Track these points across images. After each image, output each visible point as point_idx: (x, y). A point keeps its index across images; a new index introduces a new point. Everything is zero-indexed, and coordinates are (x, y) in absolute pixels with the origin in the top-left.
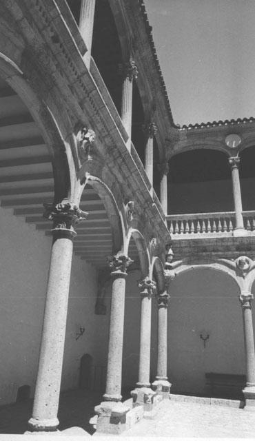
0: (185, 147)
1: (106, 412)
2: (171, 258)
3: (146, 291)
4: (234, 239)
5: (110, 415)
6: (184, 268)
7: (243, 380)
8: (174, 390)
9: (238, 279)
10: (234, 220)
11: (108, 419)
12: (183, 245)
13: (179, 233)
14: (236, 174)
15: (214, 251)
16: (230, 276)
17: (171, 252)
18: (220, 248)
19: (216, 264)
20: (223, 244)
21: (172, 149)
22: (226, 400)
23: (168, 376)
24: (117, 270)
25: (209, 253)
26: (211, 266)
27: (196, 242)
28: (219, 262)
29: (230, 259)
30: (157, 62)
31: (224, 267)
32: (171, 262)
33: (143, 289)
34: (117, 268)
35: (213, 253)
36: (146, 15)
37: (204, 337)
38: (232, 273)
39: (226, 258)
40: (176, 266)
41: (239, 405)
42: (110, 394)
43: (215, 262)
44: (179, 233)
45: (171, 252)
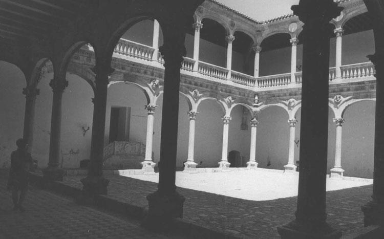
9: (289, 111)
23: (229, 161)
26: (277, 104)
28: (281, 103)
43: (278, 102)
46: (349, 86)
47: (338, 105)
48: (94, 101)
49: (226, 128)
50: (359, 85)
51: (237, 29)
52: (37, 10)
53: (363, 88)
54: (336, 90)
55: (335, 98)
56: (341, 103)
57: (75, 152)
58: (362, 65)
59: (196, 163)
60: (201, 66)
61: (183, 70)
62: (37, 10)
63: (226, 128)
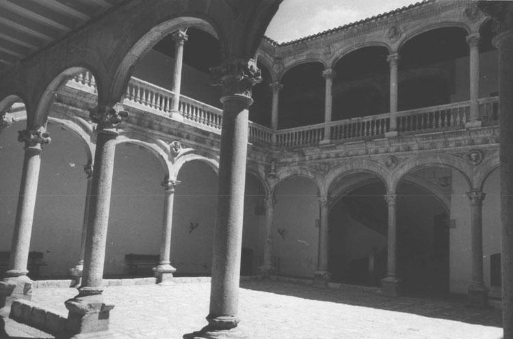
1: (94, 308)
3: (38, 147)
4: (169, 121)
5: (98, 311)
7: (157, 260)
8: (176, 275)
9: (169, 163)
10: (172, 101)
11: (97, 316)
14: (181, 50)
15: (71, 105)
18: (79, 104)
19: (70, 121)
20: (84, 99)
22: (56, 281)
23: (170, 260)
24: (113, 127)
25: (65, 106)
26: (64, 121)
28: (74, 120)
29: (87, 121)
31: (76, 125)
33: (35, 143)
34: (114, 125)
35: (71, 107)
38: (166, 157)
41: (155, 281)
42: (90, 286)
43: (69, 118)
46: (190, 132)
47: (175, 158)
48: (186, 162)
49: (172, 198)
50: (202, 136)
51: (307, 59)
52: (13, 53)
53: (202, 141)
54: (174, 132)
55: (173, 143)
56: (179, 156)
57: (24, 143)
58: (203, 106)
59: (174, 266)
60: (182, 104)
61: (128, 99)
62: (13, 53)
63: (172, 198)
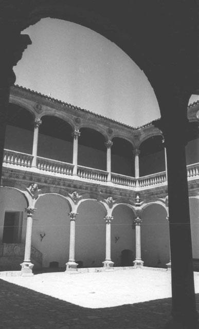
0: (145, 138)
2: (138, 200)
3: (107, 221)
6: (145, 205)
12: (143, 193)
13: (192, 176)
15: (156, 194)
16: (163, 207)
17: (138, 197)
21: (139, 140)
23: (75, 259)
26: (156, 202)
27: (148, 191)
30: (36, 93)
32: (139, 202)
35: (156, 196)
36: (27, 41)
37: (117, 238)
39: (161, 198)
40: (142, 204)
43: (157, 200)
44: (192, 176)
45: (138, 197)
